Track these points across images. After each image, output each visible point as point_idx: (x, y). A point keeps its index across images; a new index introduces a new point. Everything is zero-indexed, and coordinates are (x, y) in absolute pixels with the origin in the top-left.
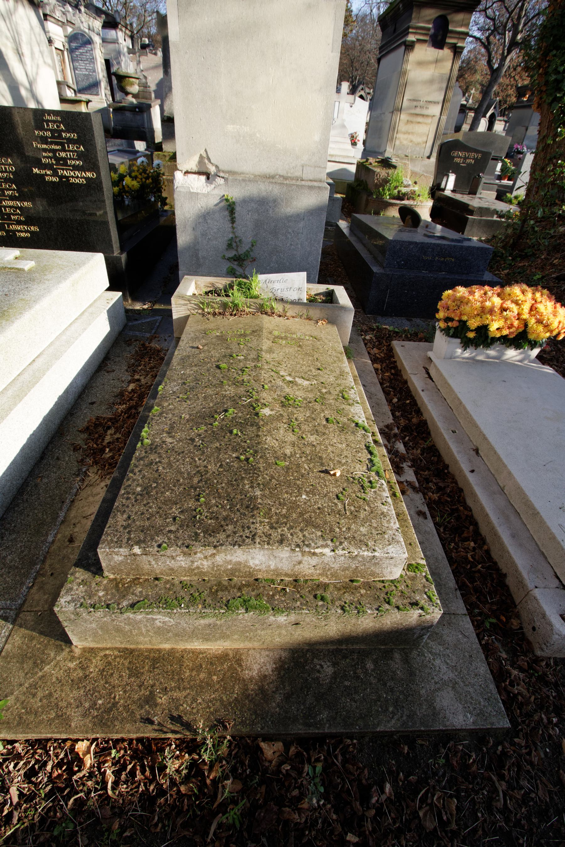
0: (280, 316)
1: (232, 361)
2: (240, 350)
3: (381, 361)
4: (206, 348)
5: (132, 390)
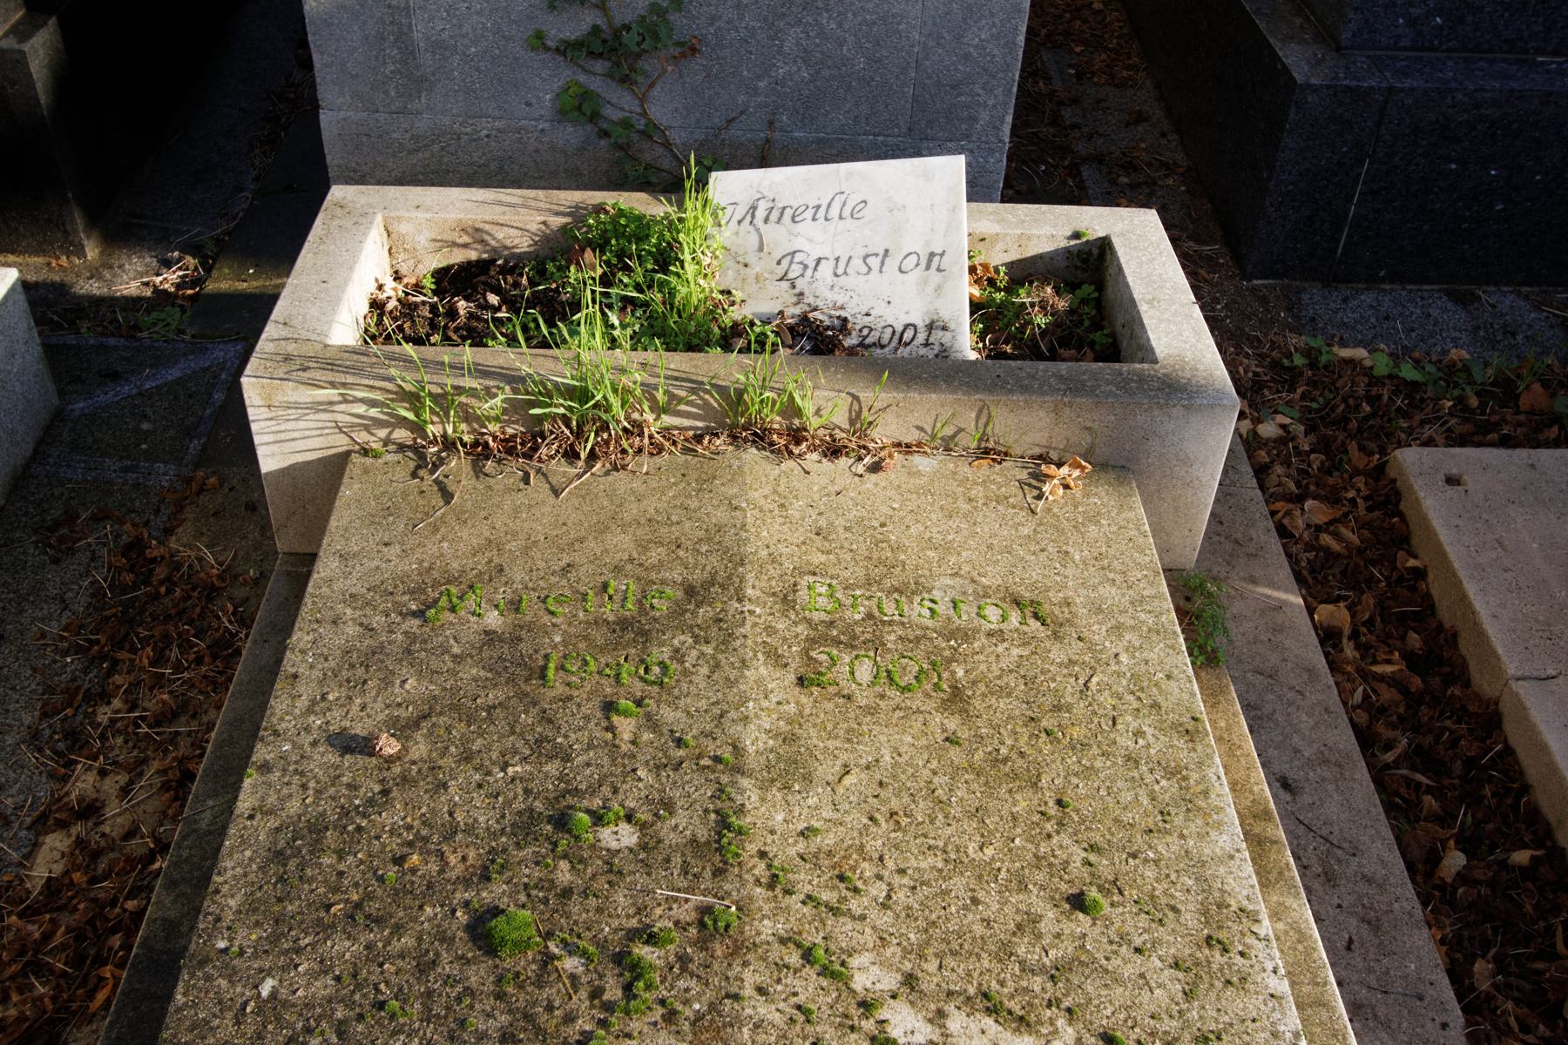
0: (833, 451)
1: (564, 874)
2: (623, 763)
3: (1355, 581)
4: (420, 748)
5: (52, 886)
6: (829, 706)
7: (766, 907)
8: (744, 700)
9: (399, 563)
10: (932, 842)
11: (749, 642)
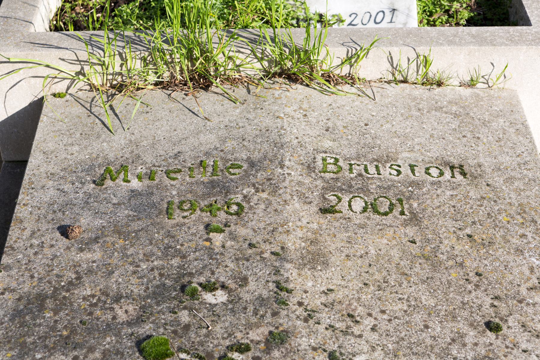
6: (337, 224)
7: (304, 331)
8: (286, 223)
9: (79, 154)
10: (400, 296)
11: (288, 190)
